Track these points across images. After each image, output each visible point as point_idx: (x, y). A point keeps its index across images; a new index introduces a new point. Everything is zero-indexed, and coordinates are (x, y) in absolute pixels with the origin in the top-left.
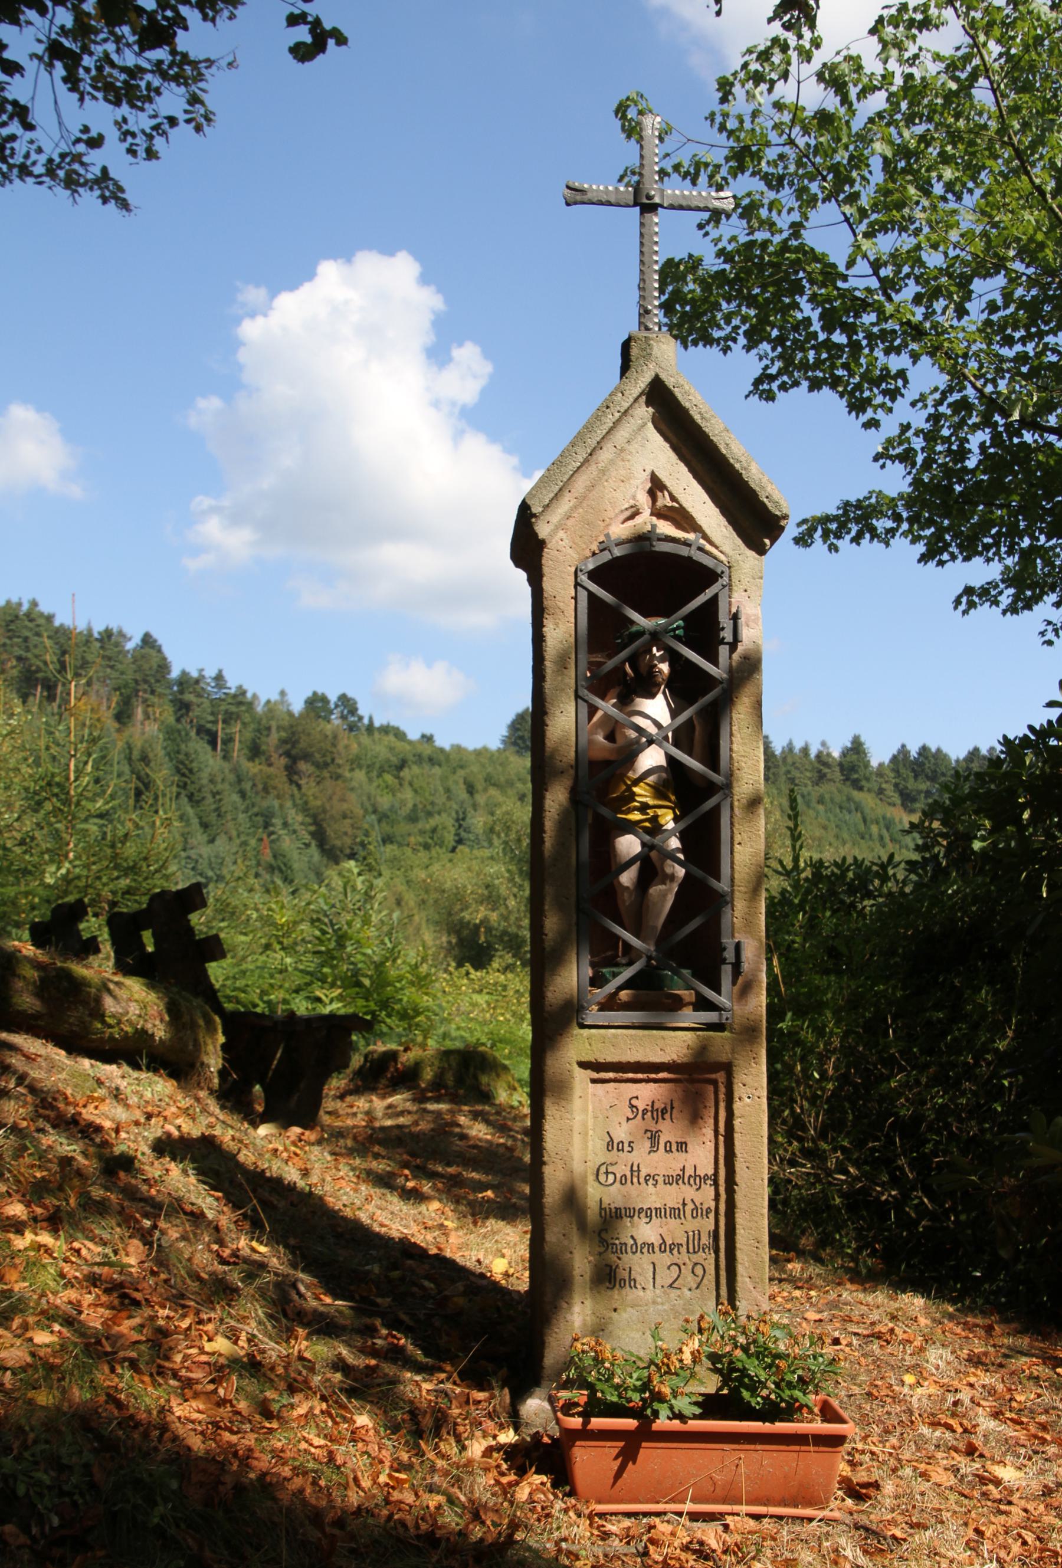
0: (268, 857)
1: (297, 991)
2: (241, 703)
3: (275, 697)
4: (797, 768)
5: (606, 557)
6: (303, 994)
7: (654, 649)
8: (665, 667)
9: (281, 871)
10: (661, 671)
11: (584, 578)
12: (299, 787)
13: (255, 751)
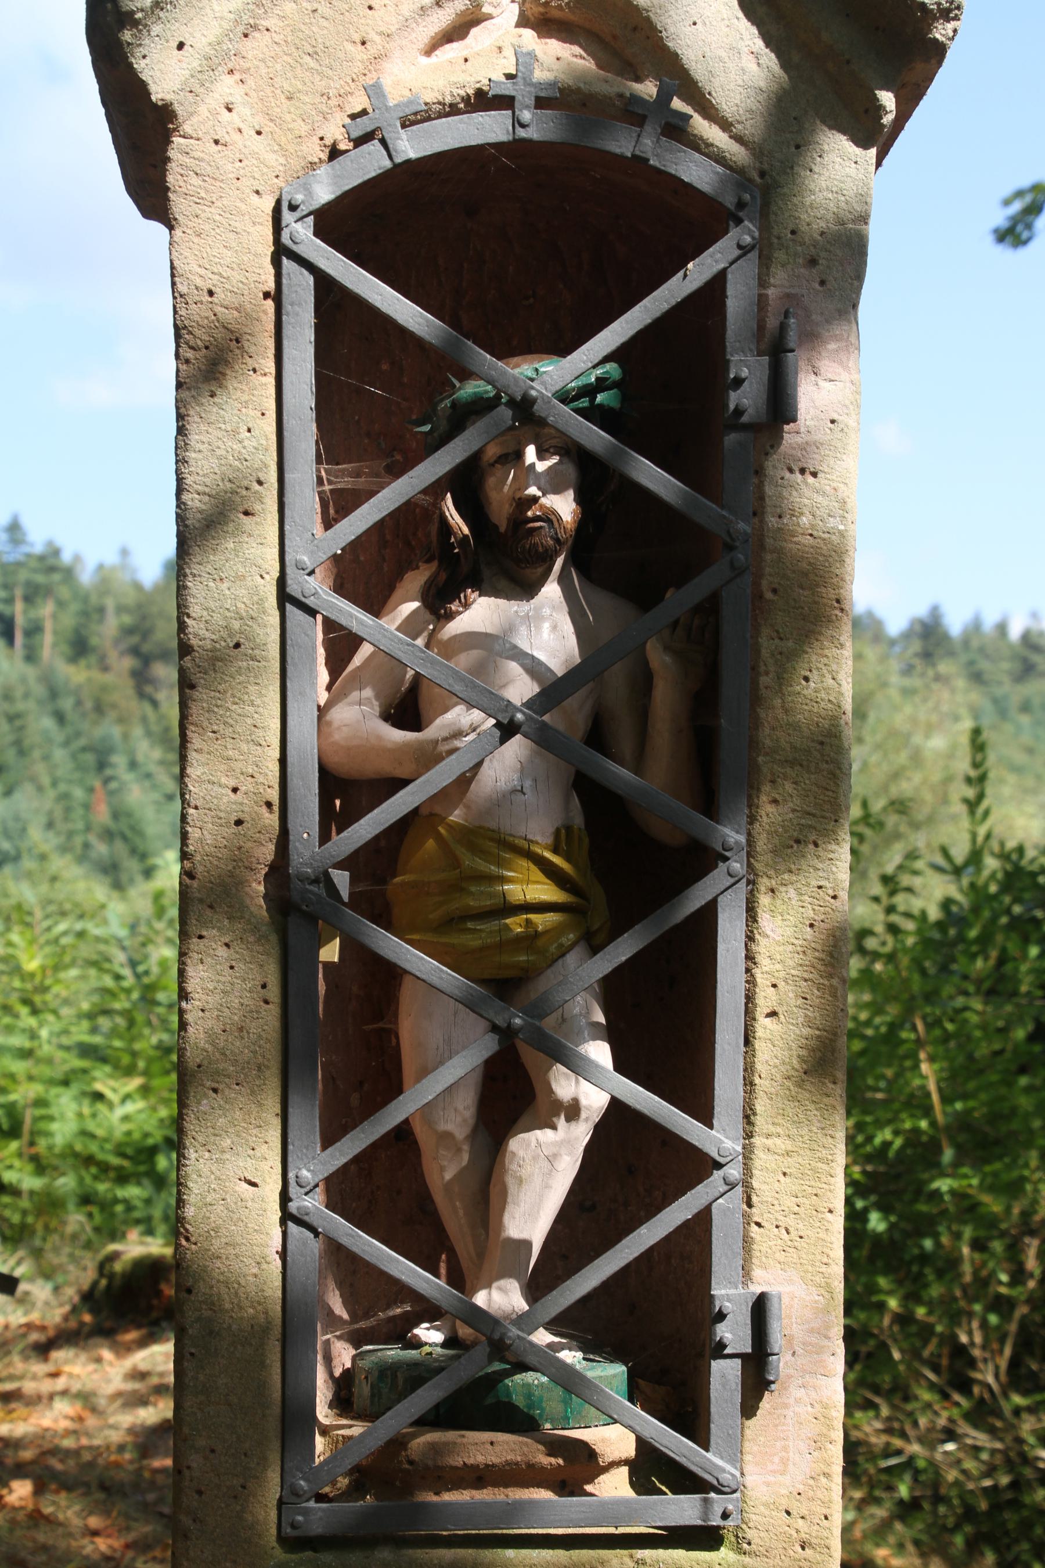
0: (102, 815)
1: (66, 1083)
2: (52, 569)
3: (111, 558)
4: (987, 657)
5: (371, 162)
6: (75, 1089)
7: (530, 453)
8: (564, 506)
9: (125, 838)
10: (550, 517)
11: (302, 233)
12: (155, 704)
13: (80, 647)
